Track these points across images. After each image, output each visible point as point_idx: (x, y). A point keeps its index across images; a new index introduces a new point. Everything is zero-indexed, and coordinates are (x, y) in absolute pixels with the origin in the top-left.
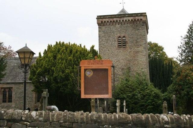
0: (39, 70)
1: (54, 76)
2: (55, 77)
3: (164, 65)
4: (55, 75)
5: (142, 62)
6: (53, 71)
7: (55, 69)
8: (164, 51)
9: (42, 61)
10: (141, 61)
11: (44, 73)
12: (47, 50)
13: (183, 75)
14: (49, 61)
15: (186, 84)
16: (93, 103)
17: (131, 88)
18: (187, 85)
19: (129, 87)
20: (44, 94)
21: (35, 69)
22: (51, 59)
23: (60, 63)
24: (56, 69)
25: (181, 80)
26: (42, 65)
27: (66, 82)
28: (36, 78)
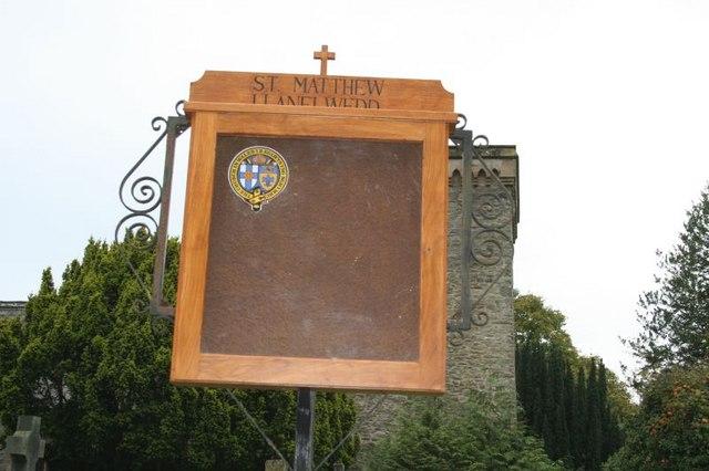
0: (35, 342)
1: (99, 376)
2: (105, 381)
3: (570, 375)
4: (104, 368)
5: (494, 350)
6: (96, 353)
7: (105, 342)
8: (563, 328)
9: (53, 306)
10: (488, 343)
11: (56, 358)
12: (81, 262)
13: (677, 408)
14: (84, 307)
15: (688, 449)
16: (245, 94)
17: (447, 457)
18: (693, 455)
19: (436, 453)
20: (18, 440)
21: (15, 341)
22: (92, 298)
23: (133, 318)
24: (111, 343)
25: (666, 431)
26: (49, 326)
27: (155, 407)
28: (16, 381)
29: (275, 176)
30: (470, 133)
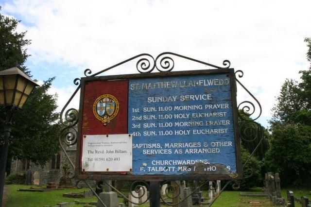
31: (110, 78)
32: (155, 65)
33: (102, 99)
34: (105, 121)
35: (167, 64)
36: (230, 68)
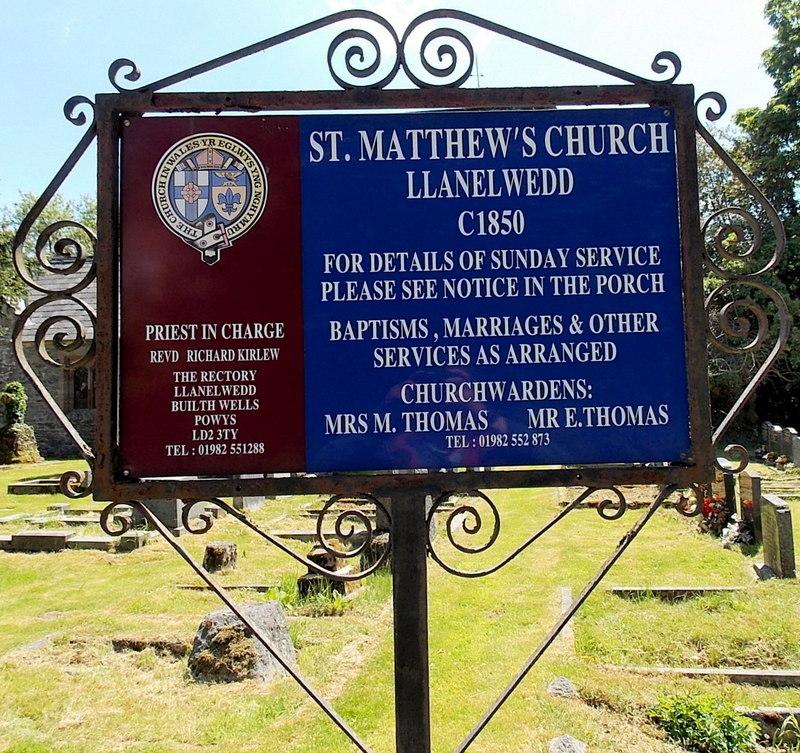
29: (242, 190)
30: (690, 88)
31: (110, 196)
32: (401, 60)
33: (193, 155)
34: (210, 240)
35: (447, 59)
36: (677, 82)
